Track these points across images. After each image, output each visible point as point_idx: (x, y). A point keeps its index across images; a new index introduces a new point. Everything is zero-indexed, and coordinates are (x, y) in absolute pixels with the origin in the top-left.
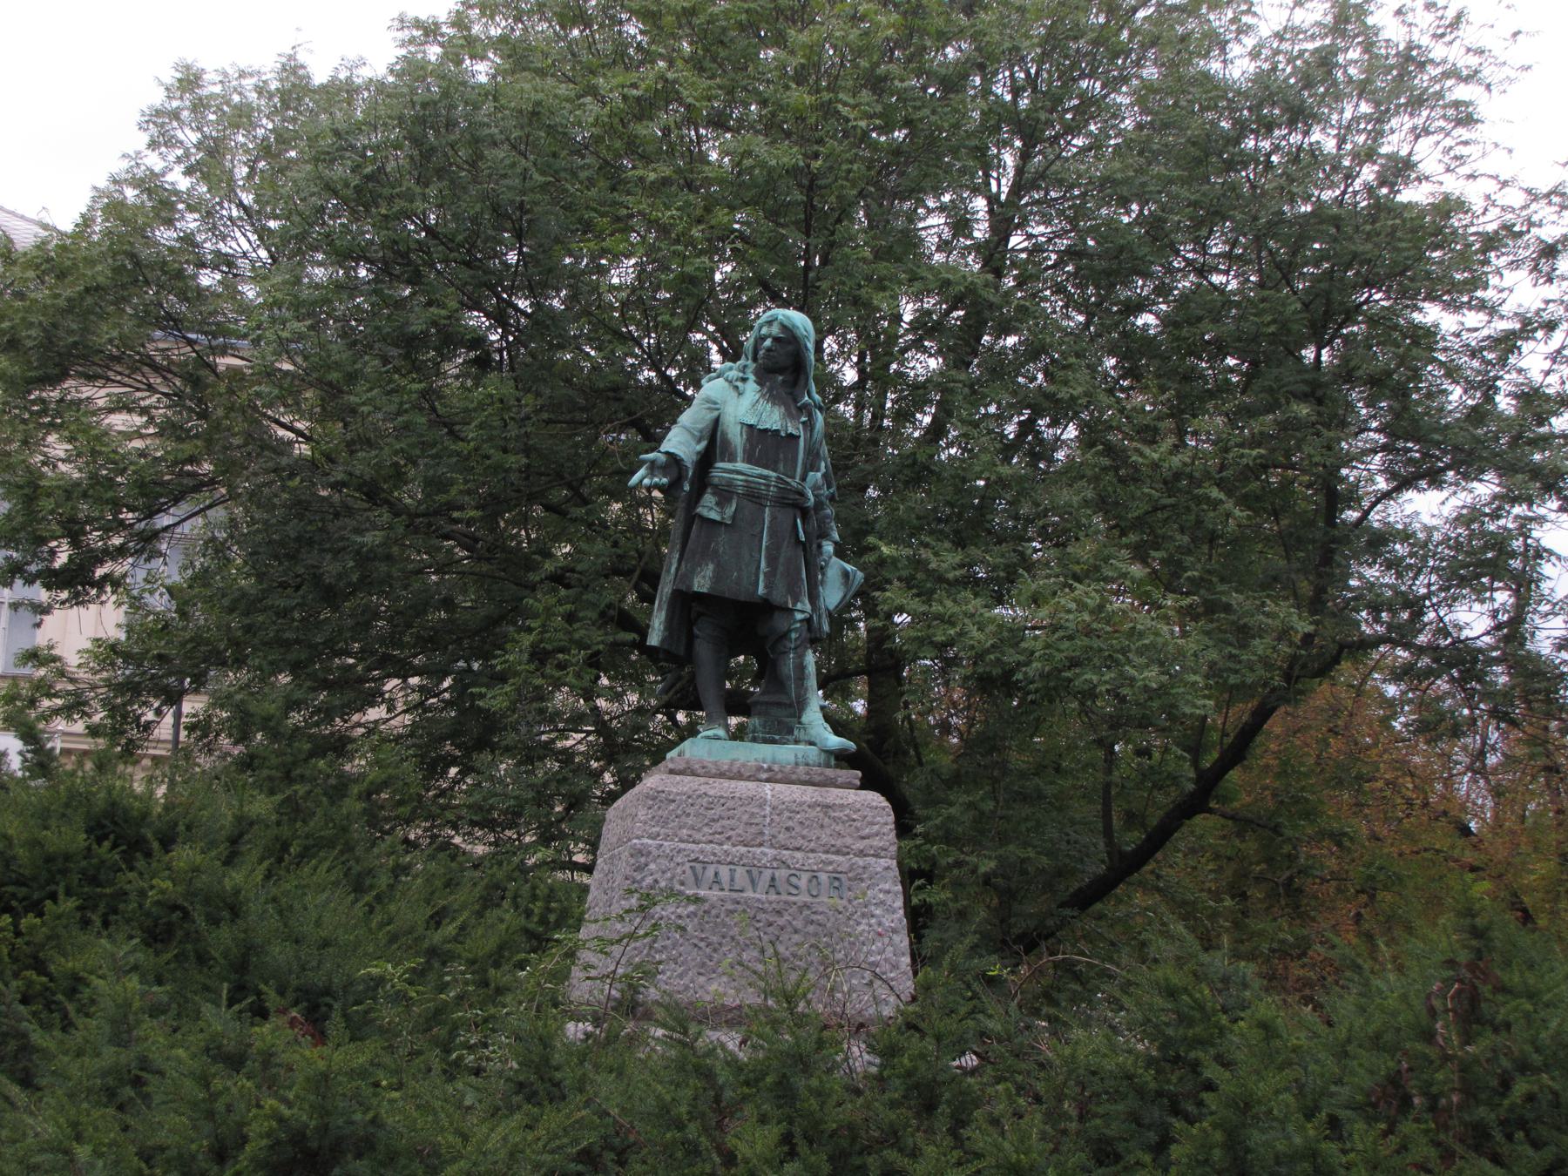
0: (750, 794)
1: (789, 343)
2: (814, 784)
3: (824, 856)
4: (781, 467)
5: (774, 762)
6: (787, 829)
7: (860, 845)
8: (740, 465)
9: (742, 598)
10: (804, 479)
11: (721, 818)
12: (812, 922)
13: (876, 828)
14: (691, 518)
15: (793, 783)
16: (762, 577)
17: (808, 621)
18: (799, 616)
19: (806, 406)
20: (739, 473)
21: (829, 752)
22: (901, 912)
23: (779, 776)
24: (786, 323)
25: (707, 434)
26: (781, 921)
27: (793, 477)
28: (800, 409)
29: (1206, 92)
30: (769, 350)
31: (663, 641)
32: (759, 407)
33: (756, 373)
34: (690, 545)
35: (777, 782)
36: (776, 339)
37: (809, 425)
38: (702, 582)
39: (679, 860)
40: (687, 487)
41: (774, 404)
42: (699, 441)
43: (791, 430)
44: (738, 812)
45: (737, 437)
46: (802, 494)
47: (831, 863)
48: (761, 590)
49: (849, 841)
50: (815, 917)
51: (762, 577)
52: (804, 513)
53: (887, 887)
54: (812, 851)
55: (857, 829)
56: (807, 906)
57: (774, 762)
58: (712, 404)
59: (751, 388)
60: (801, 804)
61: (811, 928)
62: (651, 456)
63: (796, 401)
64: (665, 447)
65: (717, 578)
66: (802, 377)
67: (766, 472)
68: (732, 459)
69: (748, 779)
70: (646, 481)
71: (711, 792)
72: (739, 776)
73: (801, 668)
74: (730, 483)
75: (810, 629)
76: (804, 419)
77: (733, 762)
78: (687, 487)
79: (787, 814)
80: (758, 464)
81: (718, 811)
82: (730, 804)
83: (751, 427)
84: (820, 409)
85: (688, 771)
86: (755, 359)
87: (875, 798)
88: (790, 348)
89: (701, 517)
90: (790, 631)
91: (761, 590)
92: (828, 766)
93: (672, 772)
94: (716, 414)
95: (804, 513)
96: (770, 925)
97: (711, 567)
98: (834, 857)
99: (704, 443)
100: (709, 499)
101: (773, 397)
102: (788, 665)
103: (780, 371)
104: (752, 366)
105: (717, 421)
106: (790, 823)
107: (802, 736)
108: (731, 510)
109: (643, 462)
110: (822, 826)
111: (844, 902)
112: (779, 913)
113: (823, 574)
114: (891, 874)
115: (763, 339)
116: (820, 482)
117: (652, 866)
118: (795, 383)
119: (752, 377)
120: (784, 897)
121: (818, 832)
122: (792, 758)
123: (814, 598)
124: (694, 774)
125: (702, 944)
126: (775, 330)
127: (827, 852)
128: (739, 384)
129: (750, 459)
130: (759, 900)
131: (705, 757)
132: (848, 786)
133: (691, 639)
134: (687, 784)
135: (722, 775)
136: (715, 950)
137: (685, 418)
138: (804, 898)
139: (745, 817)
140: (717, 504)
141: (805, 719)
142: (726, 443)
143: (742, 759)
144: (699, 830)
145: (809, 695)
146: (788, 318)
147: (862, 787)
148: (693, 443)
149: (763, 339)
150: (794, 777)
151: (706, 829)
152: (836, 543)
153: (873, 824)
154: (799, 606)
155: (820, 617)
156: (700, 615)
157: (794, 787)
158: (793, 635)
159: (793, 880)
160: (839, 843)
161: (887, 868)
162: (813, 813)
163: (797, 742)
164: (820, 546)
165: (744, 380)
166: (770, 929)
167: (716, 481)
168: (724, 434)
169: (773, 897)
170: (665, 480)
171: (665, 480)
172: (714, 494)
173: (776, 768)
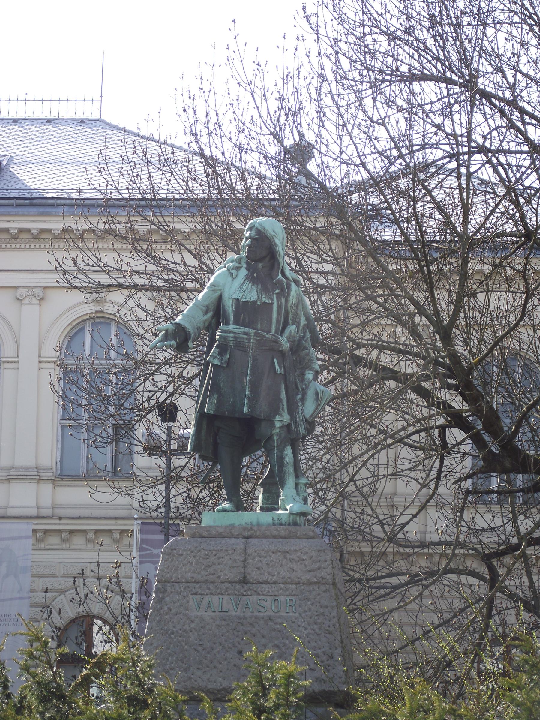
2: (281, 537)
3: (282, 586)
6: (258, 568)
7: (306, 577)
11: (214, 564)
13: (318, 565)
20: (231, 332)
25: (212, 308)
27: (269, 331)
32: (245, 287)
41: (254, 283)
42: (206, 312)
45: (229, 307)
65: (220, 402)
67: (247, 330)
68: (227, 323)
80: (243, 325)
83: (237, 300)
94: (218, 293)
99: (210, 314)
103: (260, 260)
106: (260, 565)
117: (167, 599)
122: (271, 521)
123: (292, 409)
125: (200, 649)
127: (285, 583)
129: (237, 323)
142: (225, 311)
145: (286, 477)
148: (201, 314)
155: (297, 424)
158: (275, 438)
161: (325, 591)
168: (224, 306)
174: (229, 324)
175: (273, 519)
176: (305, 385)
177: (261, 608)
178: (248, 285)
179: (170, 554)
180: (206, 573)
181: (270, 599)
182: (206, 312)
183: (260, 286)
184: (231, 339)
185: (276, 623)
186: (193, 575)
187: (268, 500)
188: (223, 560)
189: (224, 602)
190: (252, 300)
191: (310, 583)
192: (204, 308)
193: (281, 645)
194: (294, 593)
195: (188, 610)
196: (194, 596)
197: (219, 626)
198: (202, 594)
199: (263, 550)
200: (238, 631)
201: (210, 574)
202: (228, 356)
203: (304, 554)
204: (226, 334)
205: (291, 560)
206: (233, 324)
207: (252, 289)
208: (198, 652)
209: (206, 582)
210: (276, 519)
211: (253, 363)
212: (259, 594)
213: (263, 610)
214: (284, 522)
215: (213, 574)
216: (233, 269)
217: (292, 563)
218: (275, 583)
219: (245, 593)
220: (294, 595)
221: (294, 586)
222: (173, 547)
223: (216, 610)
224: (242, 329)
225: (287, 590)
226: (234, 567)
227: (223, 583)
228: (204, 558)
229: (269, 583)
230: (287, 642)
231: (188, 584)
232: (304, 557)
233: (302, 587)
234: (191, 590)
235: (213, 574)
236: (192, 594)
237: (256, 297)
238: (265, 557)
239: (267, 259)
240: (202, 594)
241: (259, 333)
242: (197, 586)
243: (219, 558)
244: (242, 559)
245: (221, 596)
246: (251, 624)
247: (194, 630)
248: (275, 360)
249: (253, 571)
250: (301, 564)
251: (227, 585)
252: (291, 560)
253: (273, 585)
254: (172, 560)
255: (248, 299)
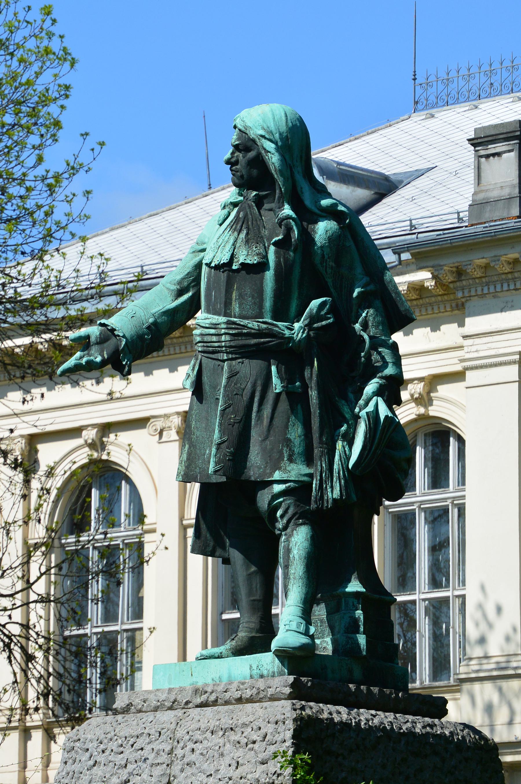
4: (236, 307)
42: (180, 293)
148: (170, 299)
154: (277, 475)
182: (180, 293)
192: (174, 287)
210: (254, 667)
214: (265, 673)
241: (234, 323)
244: (168, 748)
248: (274, 368)
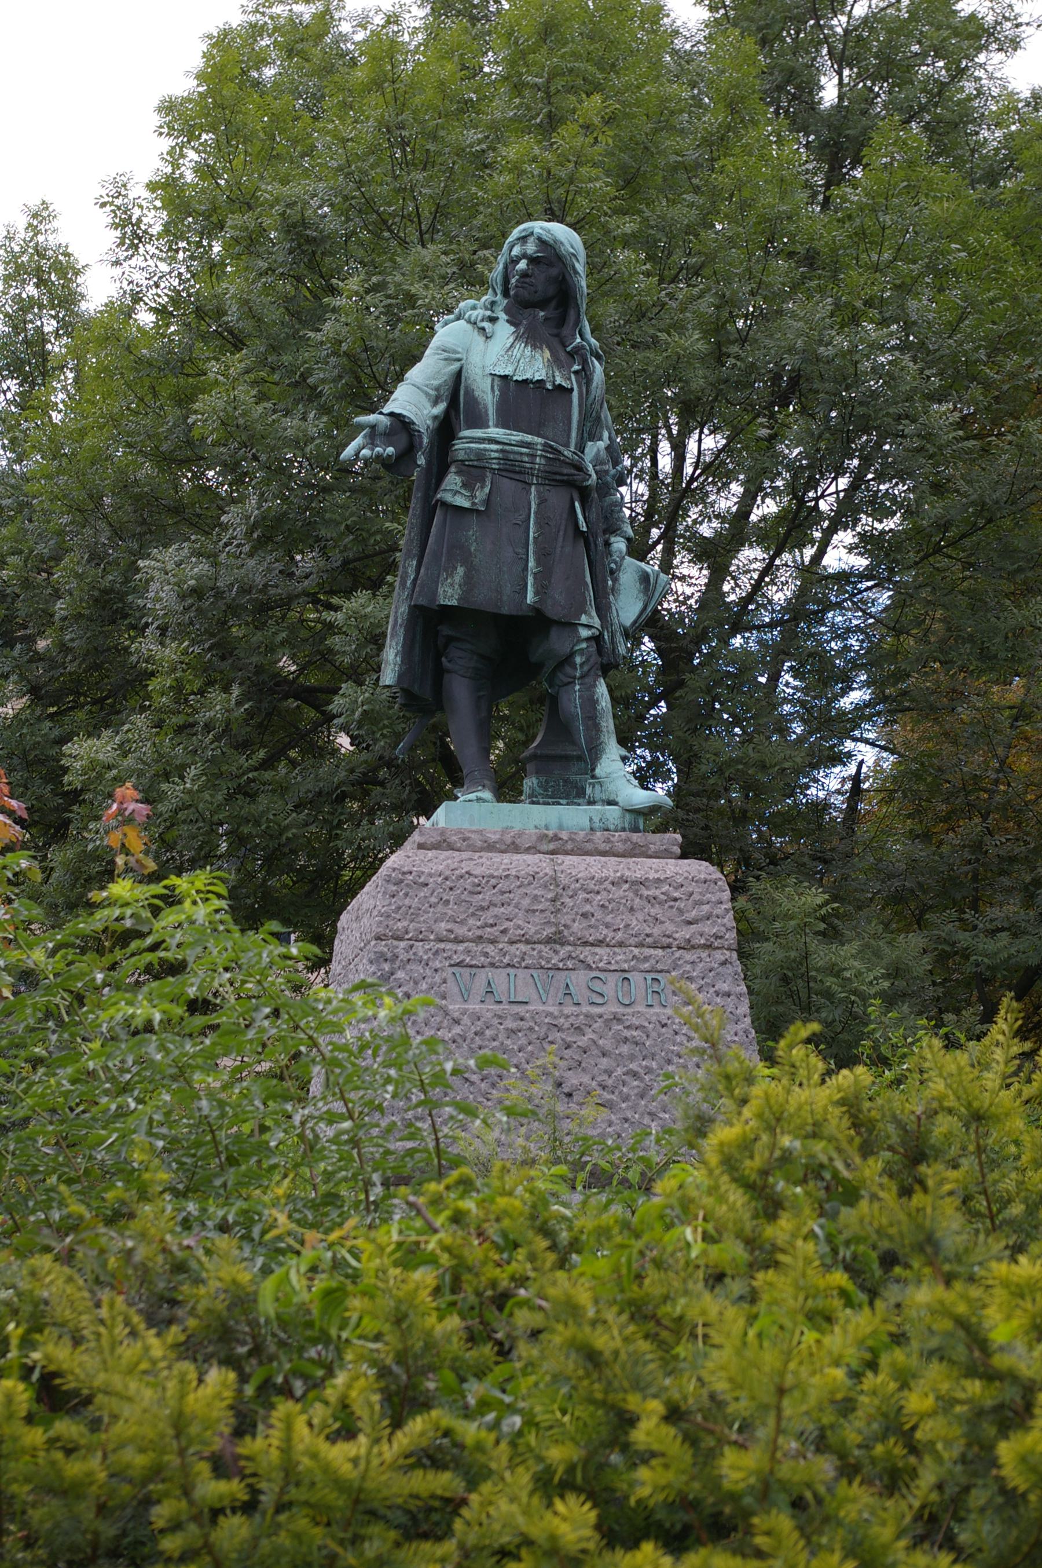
0: (531, 870)
1: (550, 265)
3: (636, 951)
5: (561, 827)
6: (584, 915)
7: (684, 933)
8: (494, 431)
9: (505, 610)
10: (581, 448)
11: (492, 904)
12: (626, 1040)
14: (431, 507)
15: (587, 853)
16: (530, 580)
17: (597, 639)
18: (584, 633)
19: (578, 349)
21: (636, 812)
22: (748, 1020)
23: (569, 846)
24: (546, 237)
25: (445, 392)
26: (583, 1041)
27: (567, 445)
28: (571, 355)
29: (504, 932)
30: (524, 275)
31: (401, 677)
32: (516, 352)
33: (507, 311)
34: (425, 560)
35: (567, 853)
36: (532, 260)
37: (585, 375)
38: (449, 594)
39: (437, 964)
40: (421, 461)
41: (534, 347)
42: (435, 402)
43: (559, 380)
44: (515, 897)
45: (487, 395)
46: (580, 468)
47: (646, 959)
48: (530, 597)
49: (669, 927)
50: (627, 1033)
51: (530, 580)
52: (584, 495)
53: (725, 987)
54: (621, 944)
55: (680, 911)
56: (617, 1018)
57: (561, 827)
58: (450, 355)
59: (504, 331)
60: (601, 881)
61: (625, 1049)
62: (372, 418)
63: (565, 346)
64: (389, 407)
65: (468, 581)
66: (572, 313)
67: (529, 438)
68: (482, 424)
69: (528, 850)
70: (366, 452)
71: (477, 871)
72: (514, 848)
73: (591, 702)
74: (480, 455)
75: (600, 651)
76: (576, 367)
77: (505, 831)
78: (421, 461)
79: (582, 895)
81: (488, 895)
82: (503, 885)
83: (505, 378)
84: (598, 358)
85: (443, 844)
86: (506, 293)
87: (699, 868)
88: (554, 272)
89: (445, 504)
90: (572, 655)
91: (530, 597)
92: (635, 829)
93: (421, 846)
94: (456, 366)
95: (584, 495)
96: (568, 1047)
97: (461, 570)
98: (652, 951)
99: (441, 407)
100: (453, 480)
101: (530, 336)
102: (573, 699)
103: (541, 304)
104: (502, 302)
105: (459, 375)
106: (588, 908)
107: (598, 795)
108: (481, 495)
109: (361, 427)
110: (632, 909)
111: (669, 1011)
112: (579, 1030)
113: (615, 580)
114: (729, 970)
115: (515, 261)
116: (603, 454)
117: (400, 975)
118: (561, 321)
119: (503, 316)
120: (586, 1009)
121: (627, 917)
123: (603, 610)
124: (451, 847)
126: (531, 248)
127: (640, 945)
128: (486, 325)
129: (504, 422)
130: (549, 1014)
131: (466, 826)
132: (665, 854)
133: (439, 673)
134: (437, 862)
135: (490, 847)
136: (493, 1085)
137: (416, 373)
138: (614, 1008)
139: (526, 902)
140: (464, 485)
141: (598, 772)
142: (473, 401)
143: (518, 827)
144: (462, 922)
146: (548, 231)
147: (684, 856)
148: (428, 405)
149: (515, 261)
150: (589, 846)
151: (471, 921)
152: (629, 540)
153: (700, 903)
154: (584, 619)
156: (450, 639)
157: (588, 858)
158: (578, 660)
159: (597, 986)
160: (656, 931)
161: (724, 963)
162: (618, 893)
163: (591, 803)
164: (607, 544)
165: (493, 320)
166: (567, 1053)
167: (461, 455)
168: (469, 392)
169: (569, 1010)
170: (390, 450)
171: (390, 450)
172: (458, 473)
173: (564, 835)
174: (488, 427)
175: (591, 819)
176: (616, 563)
177: (594, 995)
178: (520, 348)
179: (402, 881)
180: (479, 924)
181: (612, 979)
183: (547, 354)
184: (494, 455)
185: (628, 1027)
186: (449, 926)
187: (546, 790)
188: (511, 896)
189: (519, 982)
190: (537, 378)
191: (688, 946)
192: (433, 393)
193: (642, 1072)
194: (659, 967)
195: (444, 998)
196: (455, 969)
197: (512, 1032)
198: (471, 966)
199: (593, 878)
200: (552, 1043)
201: (486, 925)
202: (487, 490)
203: (676, 888)
204: (482, 446)
205: (651, 900)
206: (497, 426)
207: (533, 357)
208: (472, 1083)
209: (479, 939)
210: (596, 819)
211: (539, 505)
212: (589, 967)
213: (600, 1001)
214: (612, 827)
215: (492, 926)
216: (482, 320)
217: (653, 905)
218: (621, 944)
219: (561, 965)
220: (661, 971)
221: (659, 952)
222: (406, 869)
223: (503, 999)
224: (517, 436)
225: (646, 959)
226: (534, 911)
227: (512, 943)
228: (472, 893)
229: (608, 946)
230: (654, 1065)
231: (442, 946)
232: (676, 894)
233: (677, 955)
234: (450, 958)
235: (492, 926)
236: (451, 965)
237: (544, 373)
238: (598, 893)
239: (553, 304)
240: (471, 966)
241: (551, 447)
242: (461, 947)
243: (503, 893)
245: (512, 971)
246: (578, 1028)
247: (460, 1040)
248: (577, 504)
249: (574, 921)
250: (671, 907)
251: (523, 947)
252: (651, 900)
253: (616, 950)
254: (406, 895)
255: (528, 376)
